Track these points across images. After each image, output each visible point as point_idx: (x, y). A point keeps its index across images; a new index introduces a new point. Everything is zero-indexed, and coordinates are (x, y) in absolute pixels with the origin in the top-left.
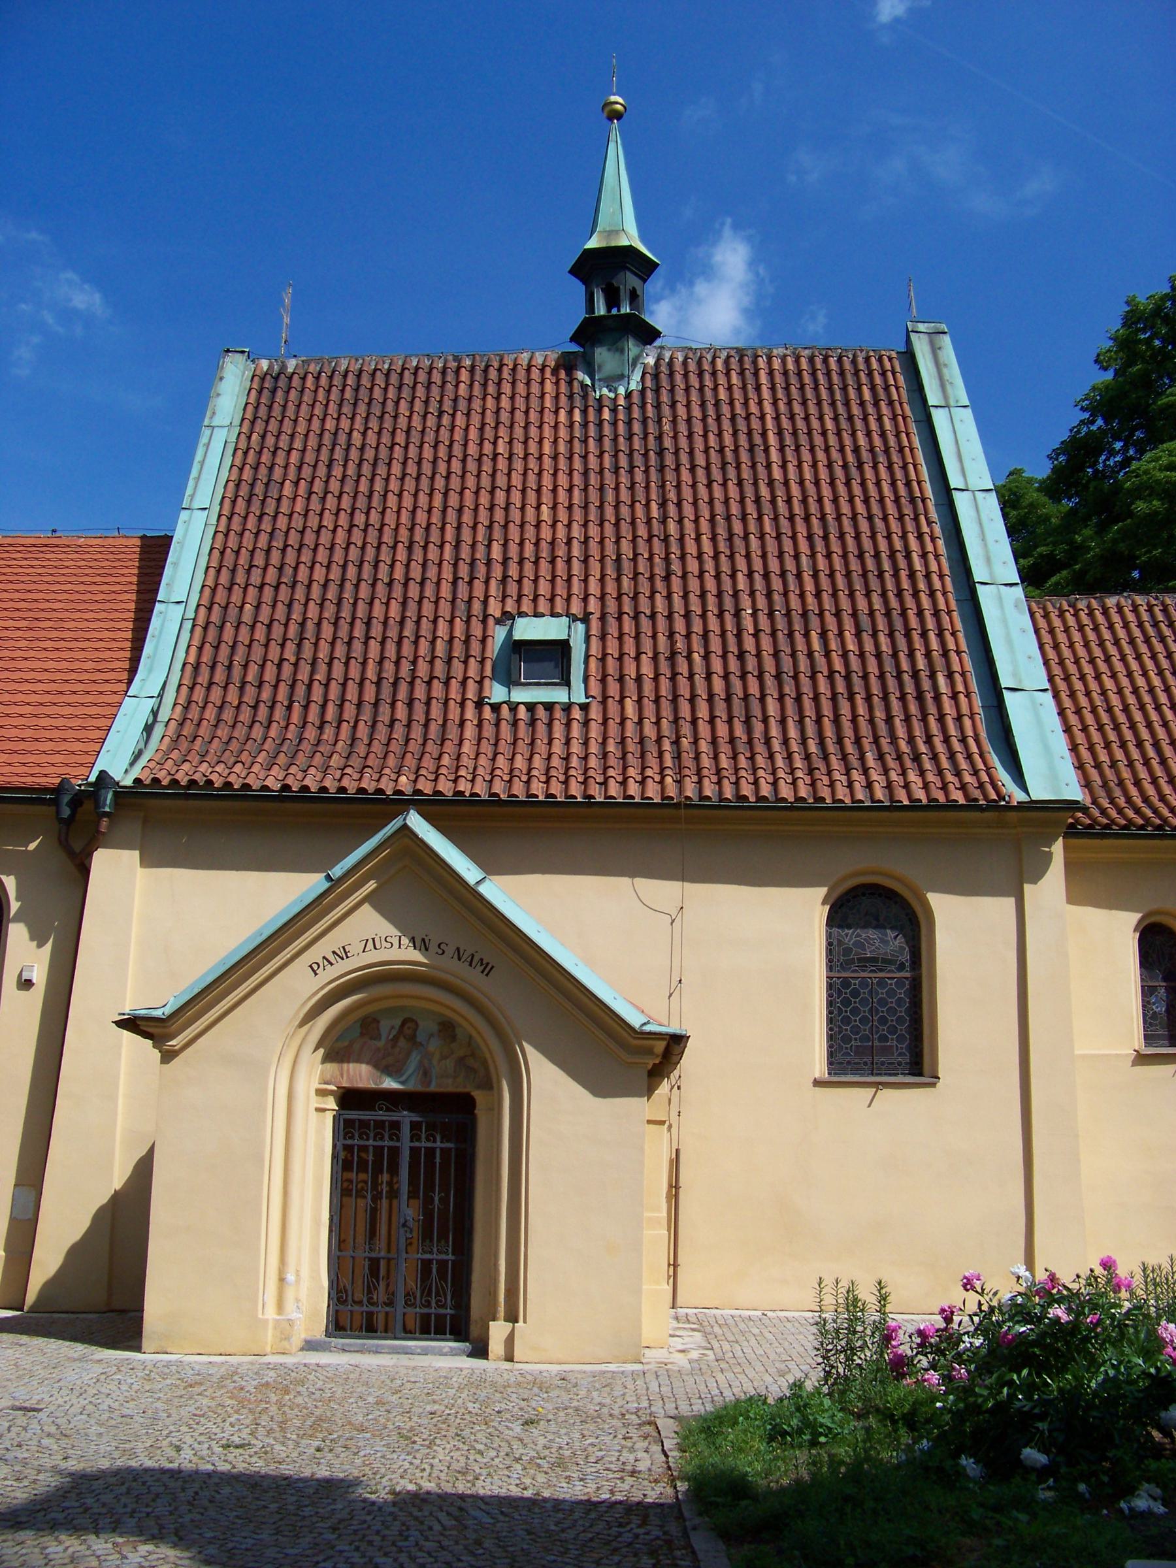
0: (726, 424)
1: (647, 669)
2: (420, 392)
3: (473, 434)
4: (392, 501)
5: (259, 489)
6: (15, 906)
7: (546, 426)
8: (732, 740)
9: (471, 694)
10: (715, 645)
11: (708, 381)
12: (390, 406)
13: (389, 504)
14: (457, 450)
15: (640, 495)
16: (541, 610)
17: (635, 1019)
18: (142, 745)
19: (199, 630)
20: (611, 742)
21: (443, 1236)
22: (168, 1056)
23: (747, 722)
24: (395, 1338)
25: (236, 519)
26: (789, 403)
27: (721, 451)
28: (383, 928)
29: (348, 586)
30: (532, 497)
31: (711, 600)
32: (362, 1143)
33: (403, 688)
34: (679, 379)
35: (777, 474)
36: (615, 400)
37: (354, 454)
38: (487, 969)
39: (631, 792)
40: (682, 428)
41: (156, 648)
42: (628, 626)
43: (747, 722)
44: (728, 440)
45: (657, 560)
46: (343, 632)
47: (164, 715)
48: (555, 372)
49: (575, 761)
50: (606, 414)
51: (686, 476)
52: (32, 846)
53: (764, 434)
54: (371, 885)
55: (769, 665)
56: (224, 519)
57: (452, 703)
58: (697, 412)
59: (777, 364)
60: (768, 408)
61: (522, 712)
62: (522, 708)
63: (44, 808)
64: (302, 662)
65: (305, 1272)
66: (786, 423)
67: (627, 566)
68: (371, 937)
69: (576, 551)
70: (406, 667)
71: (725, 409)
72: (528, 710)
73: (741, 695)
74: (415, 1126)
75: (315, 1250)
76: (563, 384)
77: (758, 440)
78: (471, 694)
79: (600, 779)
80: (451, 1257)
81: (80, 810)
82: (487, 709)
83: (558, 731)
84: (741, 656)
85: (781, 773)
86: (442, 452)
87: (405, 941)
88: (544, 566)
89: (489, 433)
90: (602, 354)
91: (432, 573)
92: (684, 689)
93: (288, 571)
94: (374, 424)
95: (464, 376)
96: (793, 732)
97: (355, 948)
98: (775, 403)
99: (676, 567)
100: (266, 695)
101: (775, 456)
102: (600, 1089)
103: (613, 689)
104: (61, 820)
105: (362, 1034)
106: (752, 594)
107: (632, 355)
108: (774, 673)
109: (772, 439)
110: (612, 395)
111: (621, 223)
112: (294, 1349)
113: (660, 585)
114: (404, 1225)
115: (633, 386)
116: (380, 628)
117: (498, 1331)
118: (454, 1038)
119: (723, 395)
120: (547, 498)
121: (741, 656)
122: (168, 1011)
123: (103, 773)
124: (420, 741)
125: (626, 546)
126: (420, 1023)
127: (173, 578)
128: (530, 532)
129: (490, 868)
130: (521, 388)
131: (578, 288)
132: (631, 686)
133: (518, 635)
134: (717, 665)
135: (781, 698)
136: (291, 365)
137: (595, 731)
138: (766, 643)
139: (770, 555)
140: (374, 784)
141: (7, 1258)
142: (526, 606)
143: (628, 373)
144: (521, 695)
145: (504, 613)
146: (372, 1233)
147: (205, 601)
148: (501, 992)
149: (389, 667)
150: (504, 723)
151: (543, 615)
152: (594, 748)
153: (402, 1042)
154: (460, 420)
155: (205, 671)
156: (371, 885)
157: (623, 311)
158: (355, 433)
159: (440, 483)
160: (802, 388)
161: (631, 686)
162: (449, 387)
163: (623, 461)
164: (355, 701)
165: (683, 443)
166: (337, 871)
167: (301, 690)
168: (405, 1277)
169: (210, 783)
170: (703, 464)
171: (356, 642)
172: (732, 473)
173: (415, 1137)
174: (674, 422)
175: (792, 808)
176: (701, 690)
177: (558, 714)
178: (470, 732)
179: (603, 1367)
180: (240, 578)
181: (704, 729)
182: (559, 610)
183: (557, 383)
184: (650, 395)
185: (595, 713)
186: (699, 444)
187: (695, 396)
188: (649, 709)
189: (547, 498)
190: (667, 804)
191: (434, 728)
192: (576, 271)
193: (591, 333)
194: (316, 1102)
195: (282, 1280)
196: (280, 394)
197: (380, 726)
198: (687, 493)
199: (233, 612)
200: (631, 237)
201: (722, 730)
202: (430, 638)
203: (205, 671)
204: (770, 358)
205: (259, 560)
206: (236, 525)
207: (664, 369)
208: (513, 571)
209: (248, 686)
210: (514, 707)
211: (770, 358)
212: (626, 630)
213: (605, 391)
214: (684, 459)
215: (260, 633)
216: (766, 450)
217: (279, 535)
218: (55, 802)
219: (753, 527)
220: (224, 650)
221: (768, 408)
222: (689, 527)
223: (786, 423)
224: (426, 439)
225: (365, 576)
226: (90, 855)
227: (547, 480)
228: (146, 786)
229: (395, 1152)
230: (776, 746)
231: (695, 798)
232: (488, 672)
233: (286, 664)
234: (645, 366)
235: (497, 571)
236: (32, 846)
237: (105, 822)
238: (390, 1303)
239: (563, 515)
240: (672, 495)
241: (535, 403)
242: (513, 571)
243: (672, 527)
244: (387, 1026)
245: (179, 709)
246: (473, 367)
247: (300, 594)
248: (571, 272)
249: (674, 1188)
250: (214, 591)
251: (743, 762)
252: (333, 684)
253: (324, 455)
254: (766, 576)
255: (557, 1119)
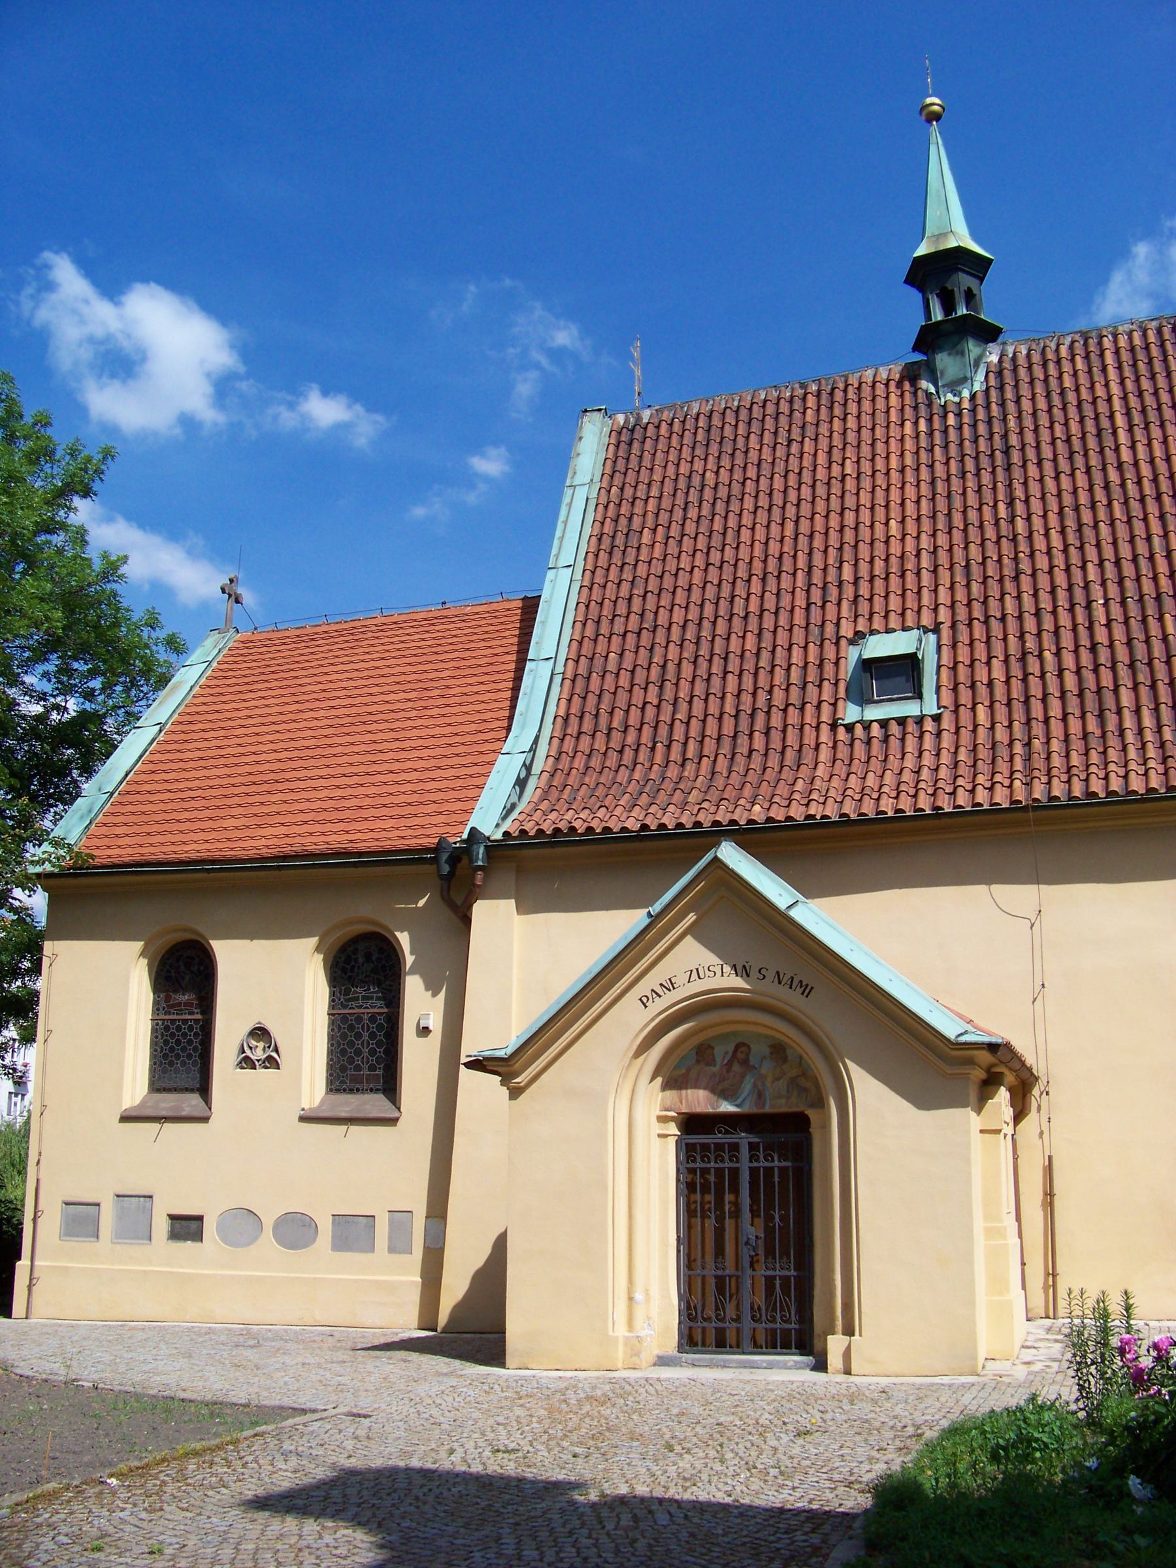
0: (1072, 412)
1: (998, 673)
2: (769, 424)
3: (822, 459)
4: (745, 535)
5: (620, 540)
6: (409, 959)
7: (892, 440)
8: (1085, 736)
9: (825, 717)
10: (1067, 640)
11: (1052, 370)
12: (741, 442)
13: (742, 539)
14: (807, 477)
15: (988, 496)
16: (892, 625)
17: (950, 1028)
18: (514, 799)
19: (568, 683)
20: (962, 750)
21: (785, 1253)
22: (515, 1093)
23: (1101, 716)
24: (744, 1353)
25: (599, 572)
26: (1137, 380)
27: (1068, 440)
28: (710, 959)
29: (706, 624)
30: (880, 513)
31: (1062, 595)
32: (703, 1165)
33: (760, 718)
34: (1022, 373)
35: (1126, 455)
36: (959, 404)
37: (708, 494)
38: (807, 990)
39: (979, 800)
40: (1028, 422)
41: (528, 706)
42: (979, 631)
43: (1101, 716)
44: (1074, 428)
45: (1006, 561)
46: (702, 671)
47: (536, 769)
48: (899, 384)
49: (925, 774)
50: (951, 420)
51: (1033, 471)
52: (421, 903)
53: (1111, 417)
54: (691, 918)
55: (1122, 653)
56: (588, 573)
57: (807, 727)
58: (1042, 404)
59: (1123, 342)
60: (1115, 389)
61: (876, 730)
62: (875, 726)
63: (427, 866)
64: (664, 703)
65: (655, 1292)
66: (1133, 401)
67: (976, 570)
68: (695, 967)
69: (925, 561)
70: (762, 697)
71: (1071, 397)
72: (882, 727)
73: (1094, 688)
74: (753, 1147)
75: (664, 1269)
76: (907, 395)
77: (1105, 423)
78: (825, 717)
79: (949, 789)
80: (793, 1273)
81: (459, 865)
82: (841, 730)
83: (911, 744)
84: (1093, 648)
85: (1132, 765)
86: (792, 480)
87: (727, 969)
88: (894, 581)
89: (837, 456)
90: (944, 361)
91: (786, 601)
92: (1035, 688)
93: (649, 616)
94: (726, 462)
95: (811, 401)
96: (1148, 721)
97: (681, 979)
98: (1122, 383)
99: (1025, 566)
100: (630, 739)
101: (1123, 437)
102: (924, 1100)
103: (965, 696)
104: (441, 877)
105: (698, 1061)
106: (1103, 583)
107: (973, 356)
108: (1127, 662)
109: (1120, 420)
110: (957, 399)
111: (950, 224)
112: (644, 1365)
113: (1009, 586)
114: (747, 1243)
115: (977, 387)
116: (738, 661)
117: (835, 1344)
118: (785, 1059)
119: (1068, 382)
120: (895, 512)
121: (1093, 648)
122: (509, 1051)
123: (473, 830)
124: (777, 769)
125: (974, 551)
126: (752, 1046)
127: (541, 637)
128: (880, 548)
129: (810, 889)
130: (867, 406)
131: (915, 296)
132: (982, 691)
133: (867, 655)
134: (1069, 661)
135: (1135, 687)
136: (646, 415)
137: (947, 741)
138: (1119, 633)
139: (1120, 541)
140: (746, 814)
141: (423, 1283)
142: (877, 623)
143: (973, 372)
144: (874, 713)
145: (856, 633)
146: (720, 1251)
147: (573, 656)
148: (819, 1011)
149: (746, 698)
150: (857, 742)
151: (894, 631)
152: (945, 758)
153: (736, 1068)
154: (808, 446)
155: (574, 721)
156: (691, 918)
157: (959, 313)
158: (708, 474)
159: (791, 511)
160: (1150, 363)
161: (982, 691)
162: (797, 414)
163: (970, 465)
164: (715, 736)
165: (1029, 437)
166: (656, 908)
167: (663, 730)
168: (752, 1294)
169: (573, 829)
170: (1050, 456)
171: (714, 678)
172: (1079, 461)
173: (752, 1158)
174: (1019, 418)
175: (1143, 800)
176: (1053, 688)
177: (911, 727)
178: (825, 754)
179: (937, 1380)
180: (604, 630)
181: (1056, 728)
182: (909, 623)
183: (902, 396)
184: (994, 394)
185: (947, 723)
186: (1045, 436)
187: (1039, 389)
188: (1001, 712)
189: (895, 512)
190: (1016, 807)
191: (790, 755)
192: (910, 280)
193: (930, 340)
194: (658, 1128)
195: (631, 1299)
196: (636, 445)
197: (738, 757)
198: (1035, 489)
199: (598, 662)
200: (962, 237)
201: (1075, 726)
202: (785, 666)
203: (574, 721)
204: (1115, 336)
205: (622, 609)
206: (599, 579)
207: (1007, 365)
208: (864, 590)
209: (614, 732)
210: (867, 726)
211: (1115, 336)
212: (977, 635)
213: (950, 396)
214: (1031, 454)
215: (624, 681)
216: (1114, 433)
217: (640, 583)
218: (435, 861)
219: (1102, 514)
220: (592, 700)
221: (1115, 389)
222: (1037, 523)
223: (1133, 401)
224: (776, 470)
225: (721, 613)
226: (470, 907)
227: (895, 495)
228: (515, 838)
229: (735, 1173)
230: (1130, 737)
231: (1044, 800)
232: (842, 693)
233: (648, 707)
234: (988, 364)
235: (849, 591)
236: (421, 903)
237: (480, 875)
238: (737, 1319)
239: (911, 527)
240: (1019, 492)
241: (880, 418)
242: (864, 590)
243: (1020, 525)
244: (721, 1052)
245: (551, 760)
246: (819, 391)
247: (660, 637)
248: (906, 282)
249: (1049, 1195)
250: (581, 643)
251: (1094, 757)
252: (694, 721)
253: (680, 500)
254: (1117, 563)
255: (882, 1134)
